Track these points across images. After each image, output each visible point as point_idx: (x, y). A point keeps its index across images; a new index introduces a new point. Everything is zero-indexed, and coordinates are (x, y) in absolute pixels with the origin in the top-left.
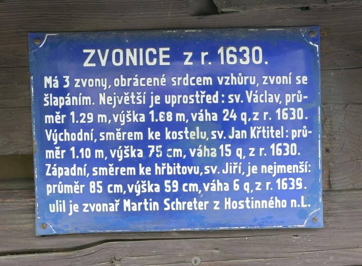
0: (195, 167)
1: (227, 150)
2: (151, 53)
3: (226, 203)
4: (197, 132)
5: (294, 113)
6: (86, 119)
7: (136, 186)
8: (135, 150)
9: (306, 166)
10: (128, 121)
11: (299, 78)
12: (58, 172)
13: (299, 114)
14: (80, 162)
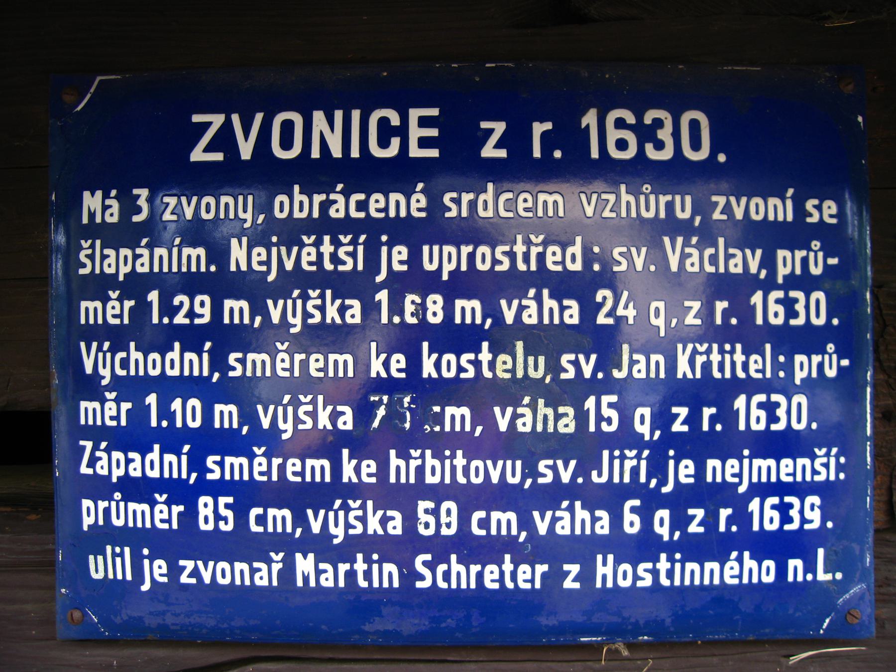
0: (509, 463)
1: (606, 412)
2: (384, 122)
3: (600, 570)
4: (518, 356)
5: (800, 307)
6: (191, 314)
7: (331, 514)
8: (330, 408)
9: (833, 461)
10: (310, 321)
11: (815, 206)
12: (112, 464)
13: (814, 308)
14: (171, 440)
